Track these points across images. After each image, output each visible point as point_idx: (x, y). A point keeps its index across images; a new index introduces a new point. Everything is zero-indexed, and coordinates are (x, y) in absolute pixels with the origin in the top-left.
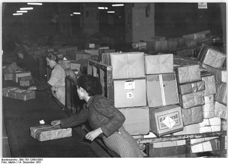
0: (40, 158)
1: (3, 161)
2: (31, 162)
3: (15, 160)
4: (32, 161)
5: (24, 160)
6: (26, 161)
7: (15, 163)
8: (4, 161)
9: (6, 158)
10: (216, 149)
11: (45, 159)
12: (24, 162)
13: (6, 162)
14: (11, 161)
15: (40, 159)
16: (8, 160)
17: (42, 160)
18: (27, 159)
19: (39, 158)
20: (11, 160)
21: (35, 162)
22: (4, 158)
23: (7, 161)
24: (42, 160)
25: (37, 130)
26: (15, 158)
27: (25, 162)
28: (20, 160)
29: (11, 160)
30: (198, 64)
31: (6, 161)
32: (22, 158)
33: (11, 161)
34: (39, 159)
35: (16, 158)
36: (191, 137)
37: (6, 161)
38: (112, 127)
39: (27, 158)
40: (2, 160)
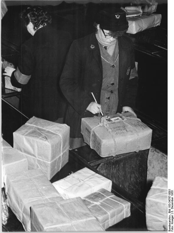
3: (170, 217)
4: (171, 199)
5: (170, 208)
6: (171, 207)
7: (168, 207)
8: (171, 229)
10: (127, 15)
11: (97, 174)
12: (172, 208)
14: (171, 222)
15: (169, 192)
16: (170, 225)
17: (170, 190)
20: (170, 222)
22: (168, 229)
24: (170, 190)
25: (60, 137)
27: (172, 207)
28: (169, 212)
29: (170, 222)
30: (87, 111)
31: (171, 227)
33: (171, 222)
34: (169, 193)
36: (108, 45)
37: (171, 227)
38: (35, 20)
40: (169, 231)
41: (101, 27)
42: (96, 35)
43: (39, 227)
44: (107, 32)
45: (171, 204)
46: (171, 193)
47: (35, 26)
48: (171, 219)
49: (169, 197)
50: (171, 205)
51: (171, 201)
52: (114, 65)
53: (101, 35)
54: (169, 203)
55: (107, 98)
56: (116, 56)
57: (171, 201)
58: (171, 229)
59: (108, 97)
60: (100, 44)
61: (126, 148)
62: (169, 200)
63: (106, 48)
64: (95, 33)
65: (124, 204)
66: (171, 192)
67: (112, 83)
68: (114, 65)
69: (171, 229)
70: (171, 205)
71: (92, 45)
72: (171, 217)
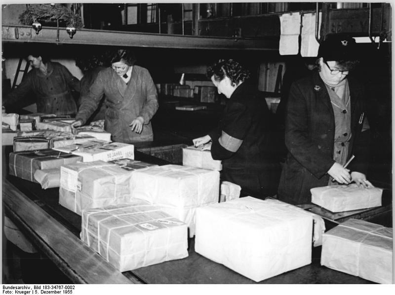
0: (70, 285)
1: (5, 289)
2: (55, 292)
3: (26, 288)
4: (57, 290)
6: (45, 290)
8: (7, 290)
9: (10, 285)
12: (42, 292)
13: (10, 292)
14: (19, 290)
15: (70, 287)
16: (14, 288)
18: (46, 287)
19: (67, 285)
20: (19, 288)
21: (62, 293)
22: (7, 285)
23: (13, 291)
26: (26, 285)
27: (45, 292)
28: (35, 287)
29: (19, 288)
31: (9, 290)
32: (39, 285)
33: (19, 290)
34: (67, 287)
35: (28, 285)
37: (9, 290)
39: (47, 285)
40: (4, 287)
41: (325, 62)
42: (320, 73)
43: (372, 240)
44: (332, 64)
45: (48, 290)
46: (67, 290)
47: (233, 81)
48: (24, 290)
49: (61, 287)
50: (47, 290)
51: (54, 290)
52: (345, 110)
53: (326, 72)
54: (51, 287)
55: (337, 152)
56: (346, 98)
57: (54, 290)
58: (6, 290)
59: (339, 151)
60: (327, 85)
61: (115, 184)
62: (56, 287)
63: (333, 89)
64: (318, 72)
65: (97, 224)
66: (70, 290)
67: (344, 133)
68: (345, 110)
69: (6, 290)
70: (47, 290)
71: (316, 86)
72: (28, 290)
